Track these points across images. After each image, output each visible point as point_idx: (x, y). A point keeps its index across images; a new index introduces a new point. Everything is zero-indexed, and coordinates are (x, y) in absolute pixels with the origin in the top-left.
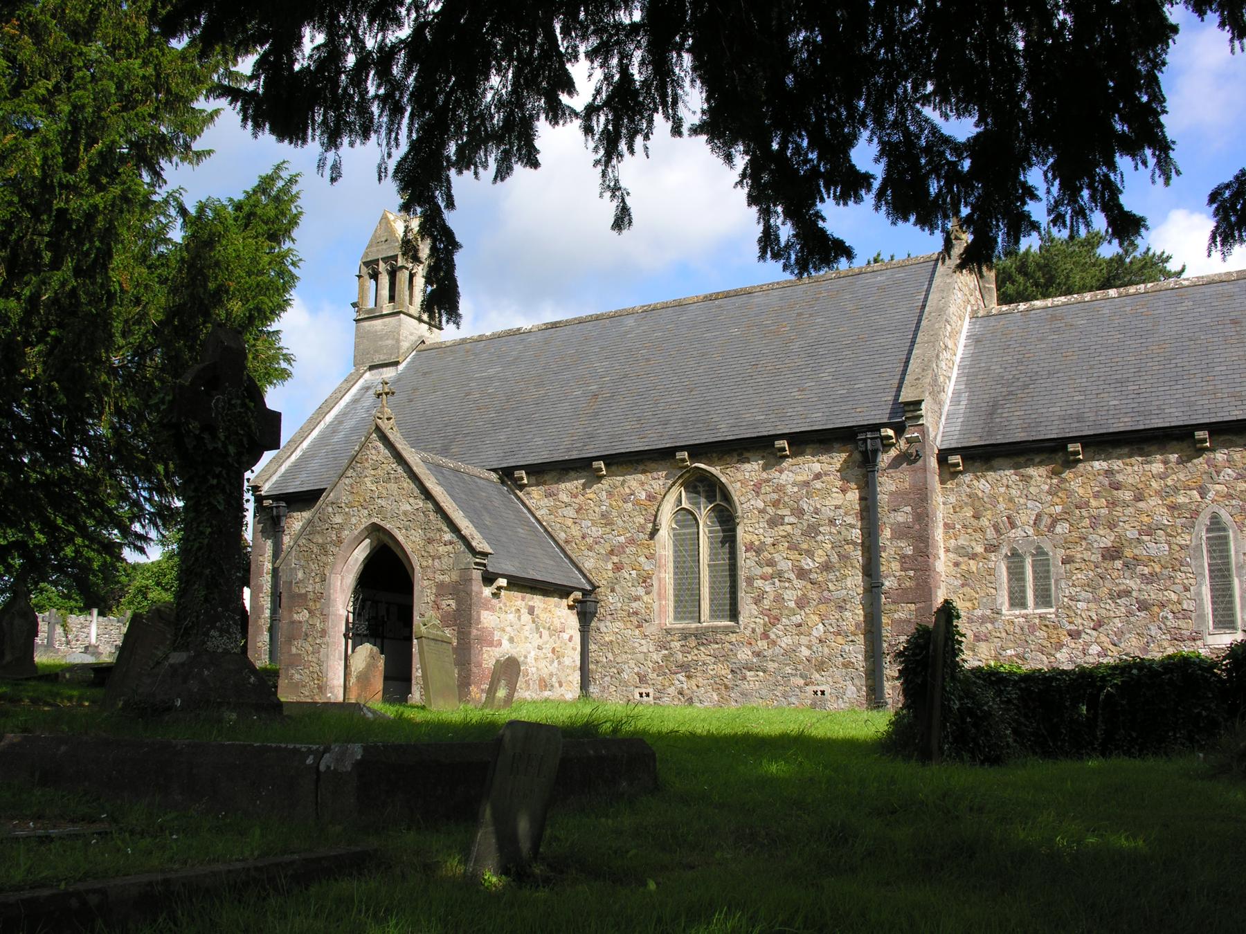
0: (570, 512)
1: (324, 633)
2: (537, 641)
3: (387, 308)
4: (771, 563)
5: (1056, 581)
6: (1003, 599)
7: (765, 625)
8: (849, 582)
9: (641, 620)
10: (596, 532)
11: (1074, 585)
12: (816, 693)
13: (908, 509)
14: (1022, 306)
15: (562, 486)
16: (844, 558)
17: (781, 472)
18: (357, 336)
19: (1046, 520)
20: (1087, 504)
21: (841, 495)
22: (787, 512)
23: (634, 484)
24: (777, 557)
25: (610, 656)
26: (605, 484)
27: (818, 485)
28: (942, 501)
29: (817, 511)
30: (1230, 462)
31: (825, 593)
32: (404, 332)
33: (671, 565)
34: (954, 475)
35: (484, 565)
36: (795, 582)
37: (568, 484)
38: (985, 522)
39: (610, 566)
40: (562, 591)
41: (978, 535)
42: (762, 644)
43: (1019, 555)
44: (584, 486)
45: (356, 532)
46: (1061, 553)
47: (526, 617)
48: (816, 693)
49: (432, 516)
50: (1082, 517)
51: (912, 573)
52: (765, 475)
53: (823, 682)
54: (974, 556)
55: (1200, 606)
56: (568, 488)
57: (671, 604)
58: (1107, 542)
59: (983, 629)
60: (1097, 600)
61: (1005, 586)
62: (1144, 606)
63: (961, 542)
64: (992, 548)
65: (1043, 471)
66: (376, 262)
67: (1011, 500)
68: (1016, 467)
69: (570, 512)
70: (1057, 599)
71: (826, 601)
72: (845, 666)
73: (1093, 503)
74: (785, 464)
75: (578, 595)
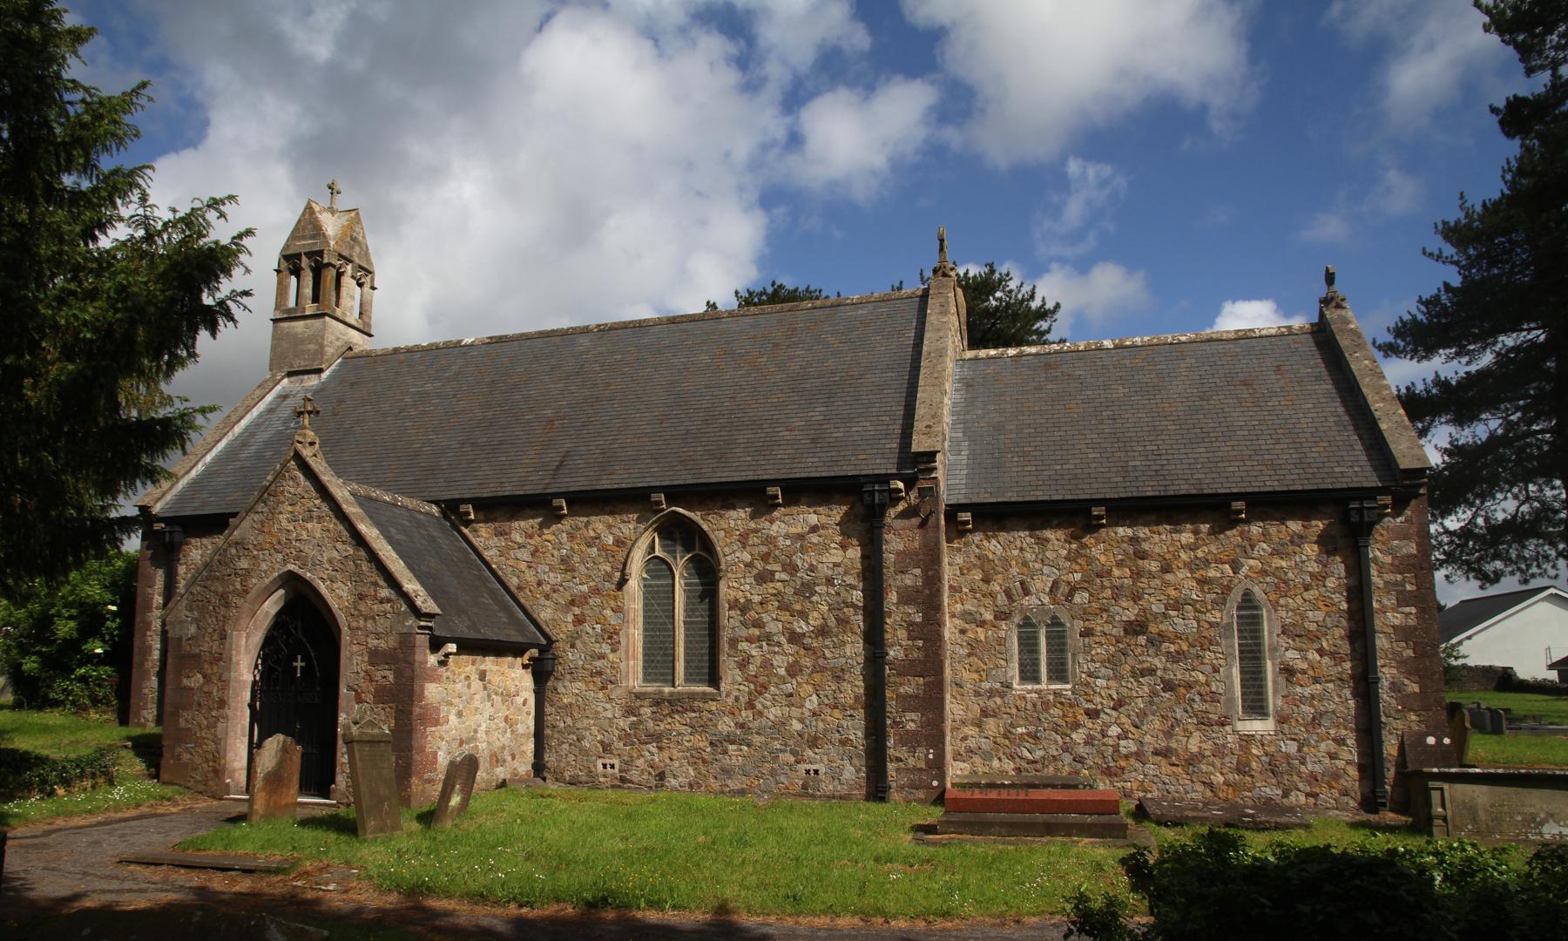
0: (524, 555)
1: (222, 703)
2: (488, 710)
3: (310, 308)
4: (758, 624)
5: (1074, 655)
6: (1014, 670)
7: (750, 693)
8: (848, 650)
9: (605, 680)
10: (554, 578)
11: (1093, 661)
12: (808, 772)
13: (918, 571)
14: (1012, 352)
15: (516, 524)
16: (843, 622)
17: (772, 522)
18: (274, 338)
19: (1064, 589)
20: (1109, 573)
21: (840, 552)
22: (777, 567)
23: (600, 527)
24: (766, 618)
25: (569, 721)
26: (566, 524)
27: (814, 539)
28: (952, 563)
29: (812, 568)
30: (1265, 535)
31: (821, 661)
32: (329, 337)
33: (641, 620)
34: (962, 533)
35: (430, 628)
36: (786, 646)
37: (523, 523)
38: (996, 587)
39: (570, 618)
40: (516, 650)
41: (988, 601)
42: (746, 715)
43: (1033, 626)
44: (542, 526)
45: (267, 581)
46: (1079, 625)
47: (476, 684)
48: (808, 772)
49: (365, 566)
50: (1103, 587)
51: (920, 643)
52: (752, 525)
53: (817, 761)
54: (982, 624)
55: (1229, 688)
56: (520, 528)
57: (640, 663)
58: (1131, 614)
59: (991, 703)
60: (1118, 678)
61: (1016, 658)
62: (1169, 686)
63: (968, 607)
64: (1002, 616)
65: (1061, 534)
66: (298, 256)
67: (1025, 564)
68: (1032, 528)
69: (524, 555)
70: (1074, 675)
71: (823, 670)
72: (843, 743)
73: (1116, 572)
74: (776, 514)
75: (534, 652)
